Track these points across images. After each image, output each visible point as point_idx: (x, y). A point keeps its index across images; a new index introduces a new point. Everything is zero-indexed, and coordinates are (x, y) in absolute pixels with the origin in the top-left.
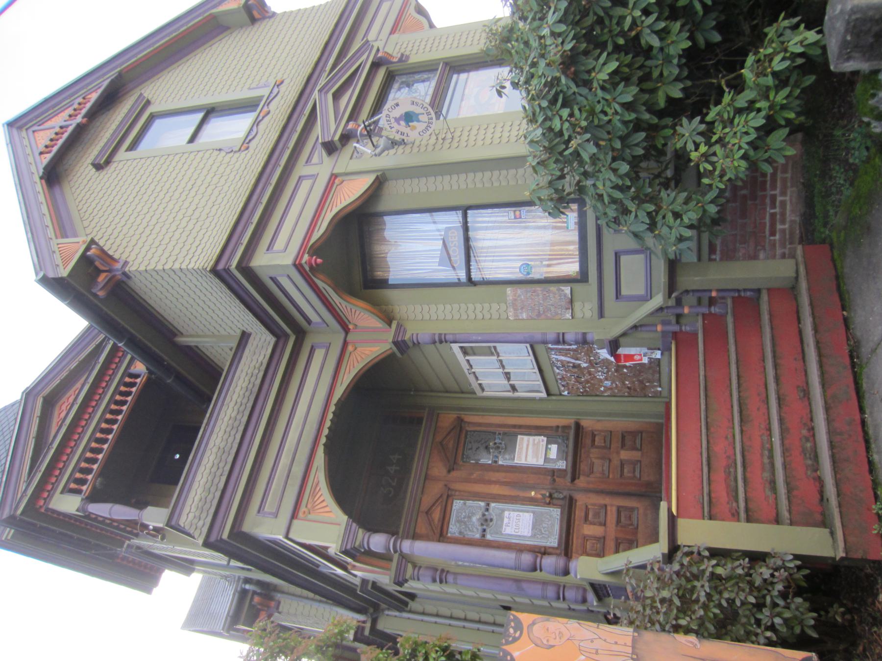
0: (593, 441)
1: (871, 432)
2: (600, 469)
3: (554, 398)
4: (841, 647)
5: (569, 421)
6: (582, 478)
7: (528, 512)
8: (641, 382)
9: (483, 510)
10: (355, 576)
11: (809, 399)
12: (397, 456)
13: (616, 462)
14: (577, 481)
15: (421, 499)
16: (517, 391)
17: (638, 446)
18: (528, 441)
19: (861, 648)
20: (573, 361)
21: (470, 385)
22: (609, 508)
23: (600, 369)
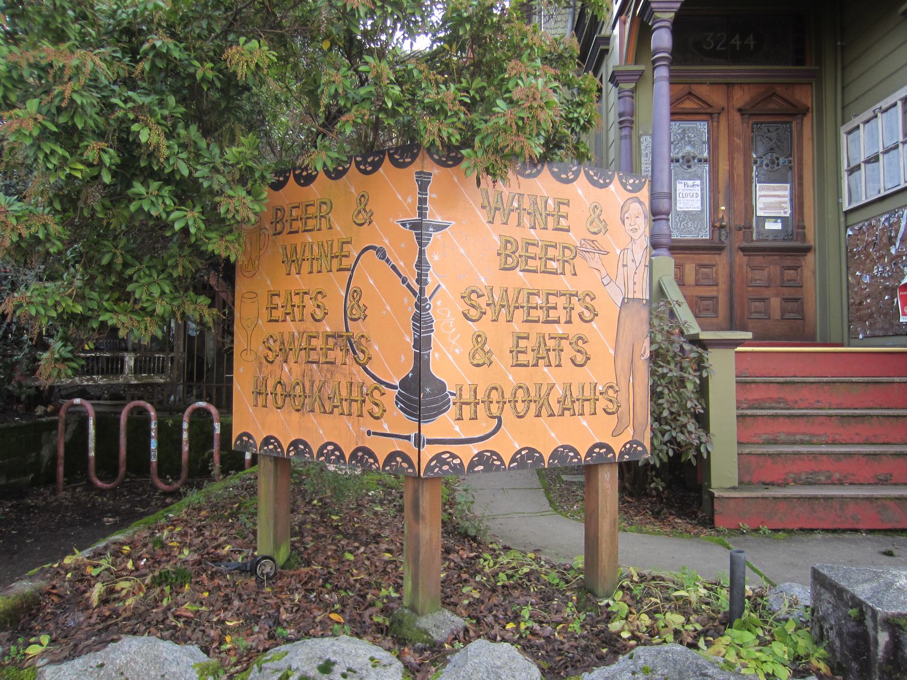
0: (789, 268)
1: (846, 536)
2: (757, 277)
3: (842, 219)
4: (627, 484)
5: (811, 237)
6: (745, 259)
7: (702, 205)
8: (871, 316)
9: (700, 156)
10: (614, 27)
11: (877, 484)
12: (752, 43)
13: (766, 293)
14: (741, 253)
15: (705, 83)
16: (849, 175)
17: (787, 316)
18: (784, 196)
19: (629, 500)
20: (900, 236)
21: (856, 115)
22: (715, 288)
23: (888, 268)
